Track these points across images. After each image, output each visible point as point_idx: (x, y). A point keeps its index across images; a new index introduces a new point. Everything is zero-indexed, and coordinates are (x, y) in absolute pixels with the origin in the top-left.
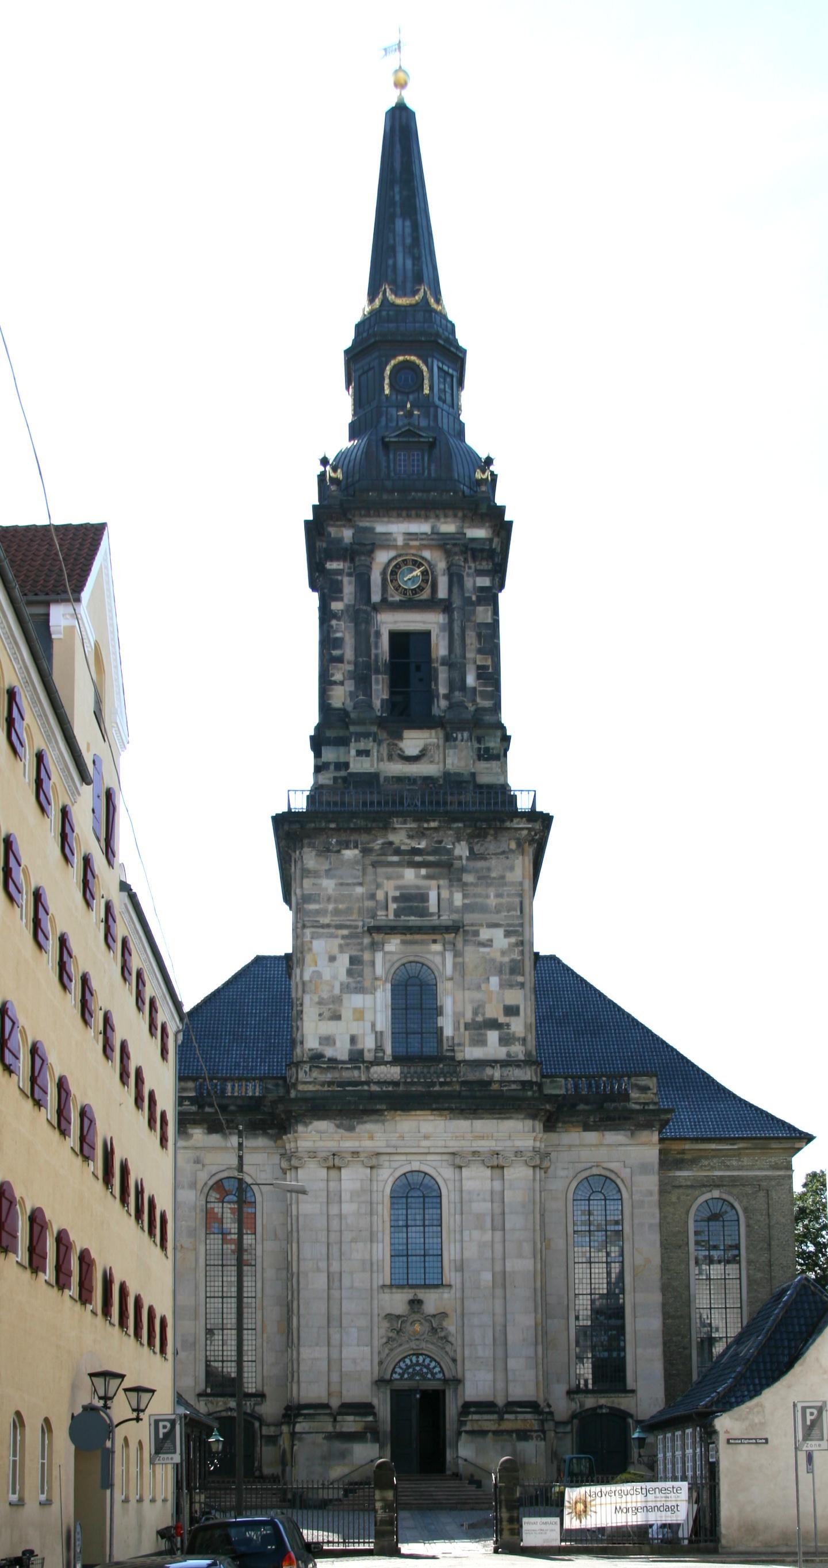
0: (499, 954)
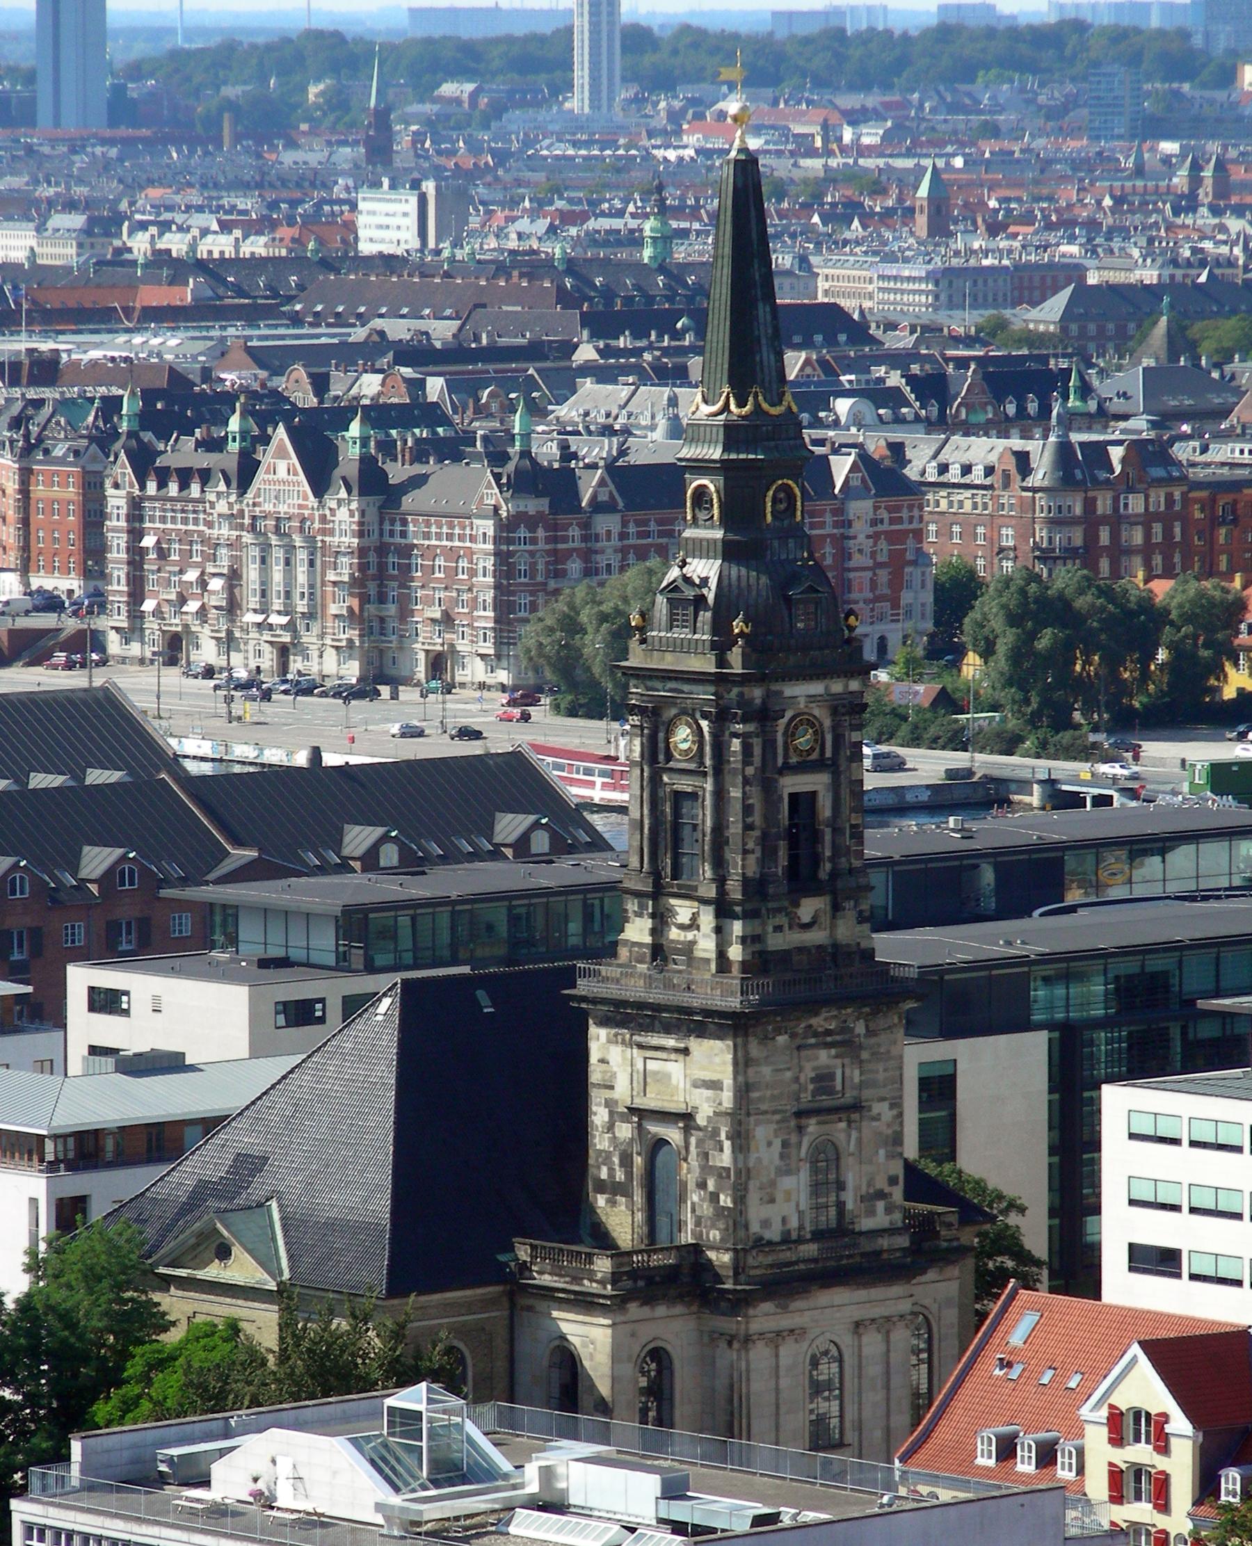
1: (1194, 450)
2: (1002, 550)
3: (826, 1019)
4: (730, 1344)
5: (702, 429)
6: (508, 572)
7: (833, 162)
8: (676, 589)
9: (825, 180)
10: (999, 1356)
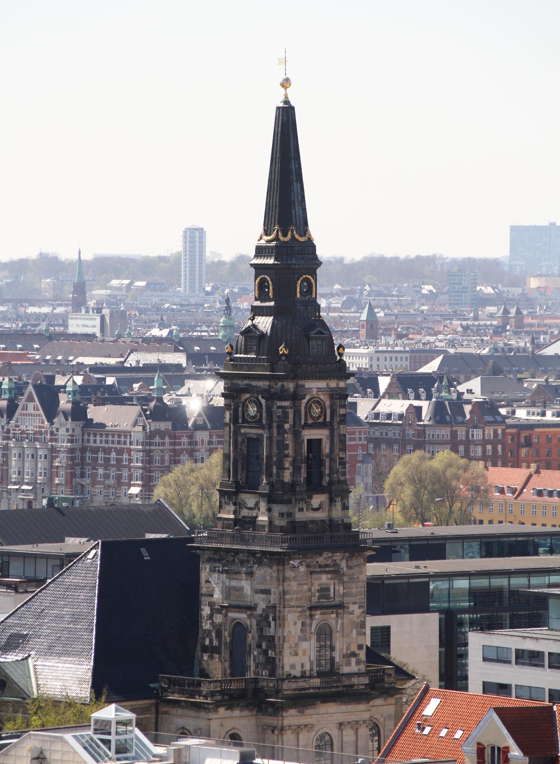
0: (356, 618)
4: (273, 732)
6: (150, 460)
10: (418, 722)
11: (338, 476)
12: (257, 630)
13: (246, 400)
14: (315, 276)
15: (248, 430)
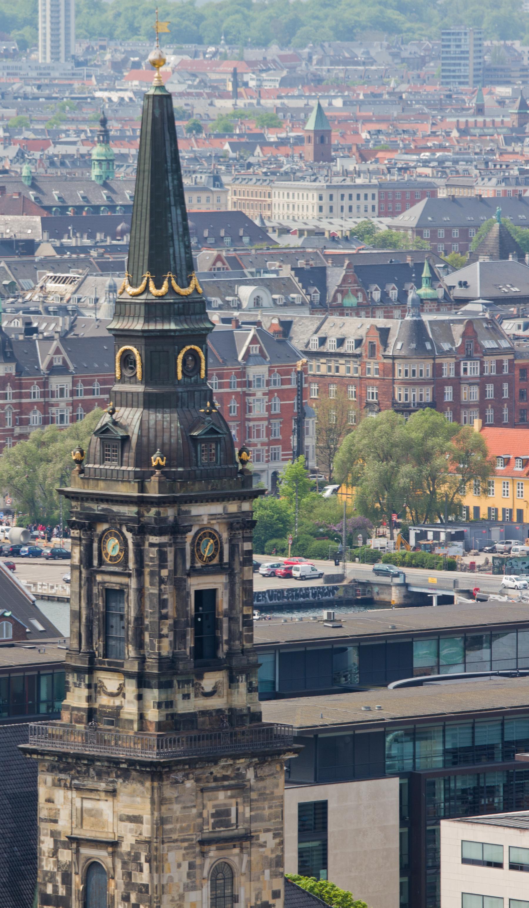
0: (270, 852)
1: (519, 327)
2: (368, 404)
3: (223, 767)
5: (128, 306)
7: (241, 103)
8: (107, 431)
9: (234, 116)
11: (241, 643)
12: (123, 875)
13: (104, 532)
14: (204, 346)
15: (107, 578)
